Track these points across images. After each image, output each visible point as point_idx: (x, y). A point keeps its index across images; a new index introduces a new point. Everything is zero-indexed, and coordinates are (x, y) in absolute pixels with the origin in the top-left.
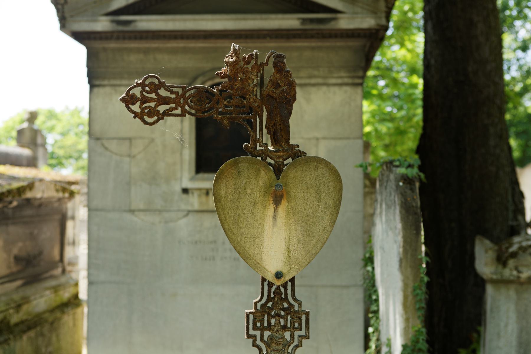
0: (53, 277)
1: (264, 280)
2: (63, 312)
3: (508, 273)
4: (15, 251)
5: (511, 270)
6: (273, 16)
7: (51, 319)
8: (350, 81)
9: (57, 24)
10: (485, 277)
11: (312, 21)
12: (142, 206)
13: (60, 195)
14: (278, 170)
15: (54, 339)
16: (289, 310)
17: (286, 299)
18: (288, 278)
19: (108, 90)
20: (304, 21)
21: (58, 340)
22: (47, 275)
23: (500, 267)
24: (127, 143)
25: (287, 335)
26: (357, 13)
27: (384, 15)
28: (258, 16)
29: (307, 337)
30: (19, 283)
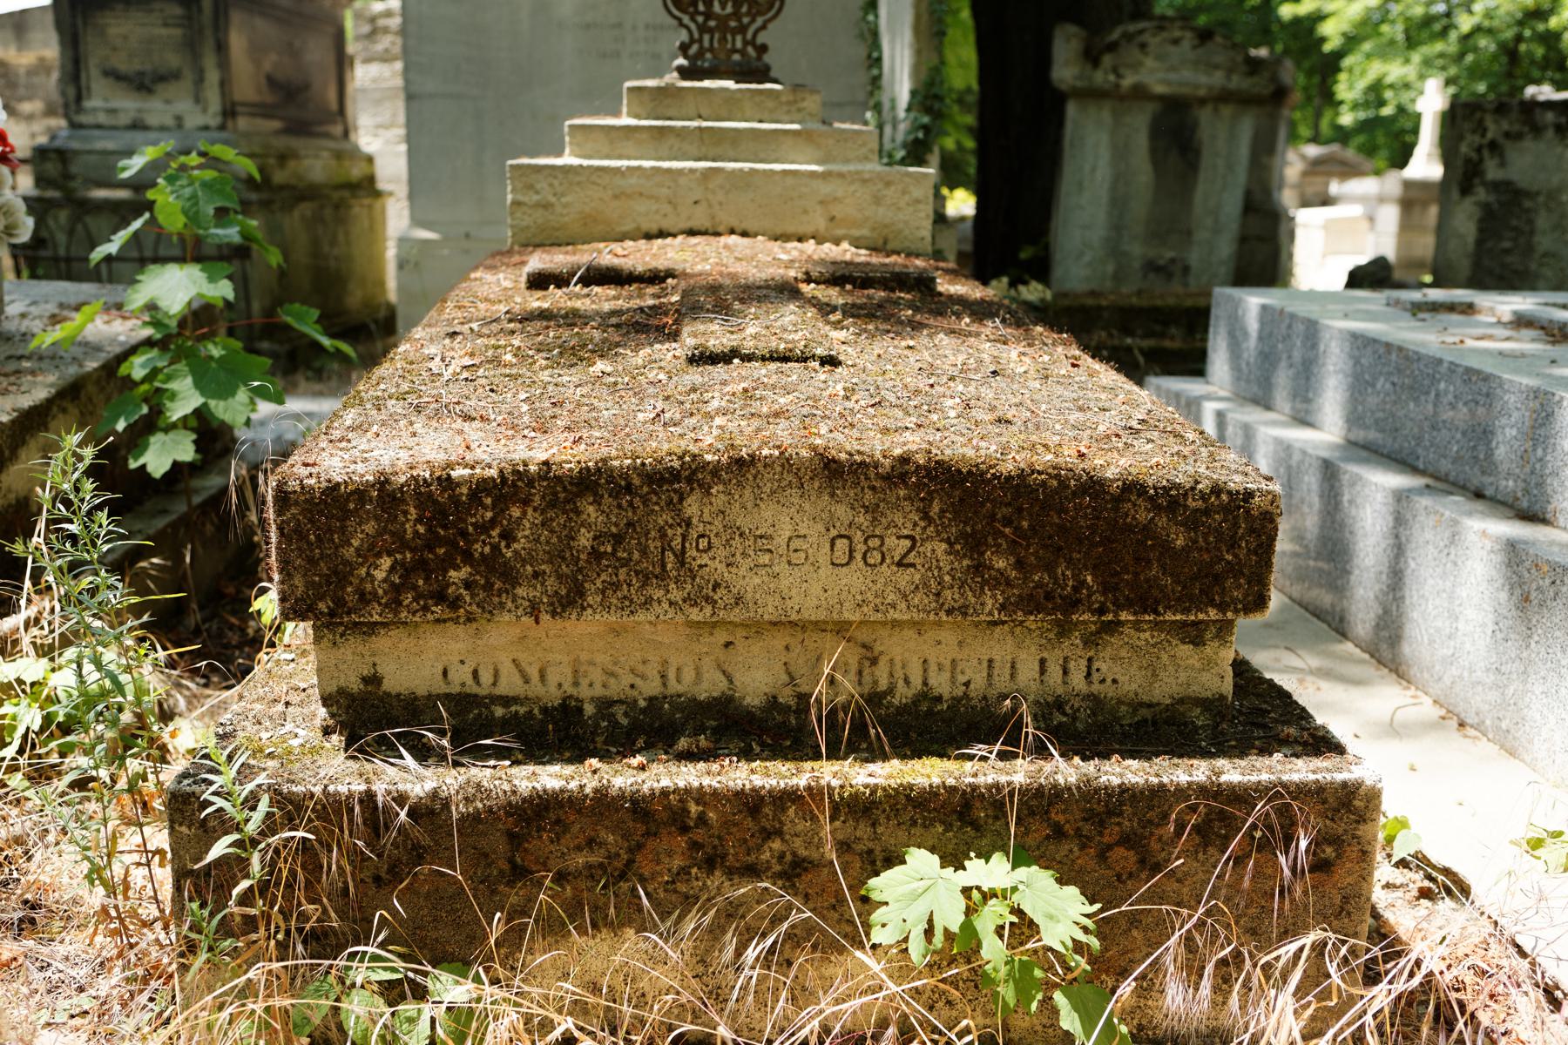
0: (327, 136)
2: (354, 196)
3: (1102, 77)
4: (267, 66)
5: (1106, 73)
10: (1063, 87)
15: (341, 237)
30: (276, 124)
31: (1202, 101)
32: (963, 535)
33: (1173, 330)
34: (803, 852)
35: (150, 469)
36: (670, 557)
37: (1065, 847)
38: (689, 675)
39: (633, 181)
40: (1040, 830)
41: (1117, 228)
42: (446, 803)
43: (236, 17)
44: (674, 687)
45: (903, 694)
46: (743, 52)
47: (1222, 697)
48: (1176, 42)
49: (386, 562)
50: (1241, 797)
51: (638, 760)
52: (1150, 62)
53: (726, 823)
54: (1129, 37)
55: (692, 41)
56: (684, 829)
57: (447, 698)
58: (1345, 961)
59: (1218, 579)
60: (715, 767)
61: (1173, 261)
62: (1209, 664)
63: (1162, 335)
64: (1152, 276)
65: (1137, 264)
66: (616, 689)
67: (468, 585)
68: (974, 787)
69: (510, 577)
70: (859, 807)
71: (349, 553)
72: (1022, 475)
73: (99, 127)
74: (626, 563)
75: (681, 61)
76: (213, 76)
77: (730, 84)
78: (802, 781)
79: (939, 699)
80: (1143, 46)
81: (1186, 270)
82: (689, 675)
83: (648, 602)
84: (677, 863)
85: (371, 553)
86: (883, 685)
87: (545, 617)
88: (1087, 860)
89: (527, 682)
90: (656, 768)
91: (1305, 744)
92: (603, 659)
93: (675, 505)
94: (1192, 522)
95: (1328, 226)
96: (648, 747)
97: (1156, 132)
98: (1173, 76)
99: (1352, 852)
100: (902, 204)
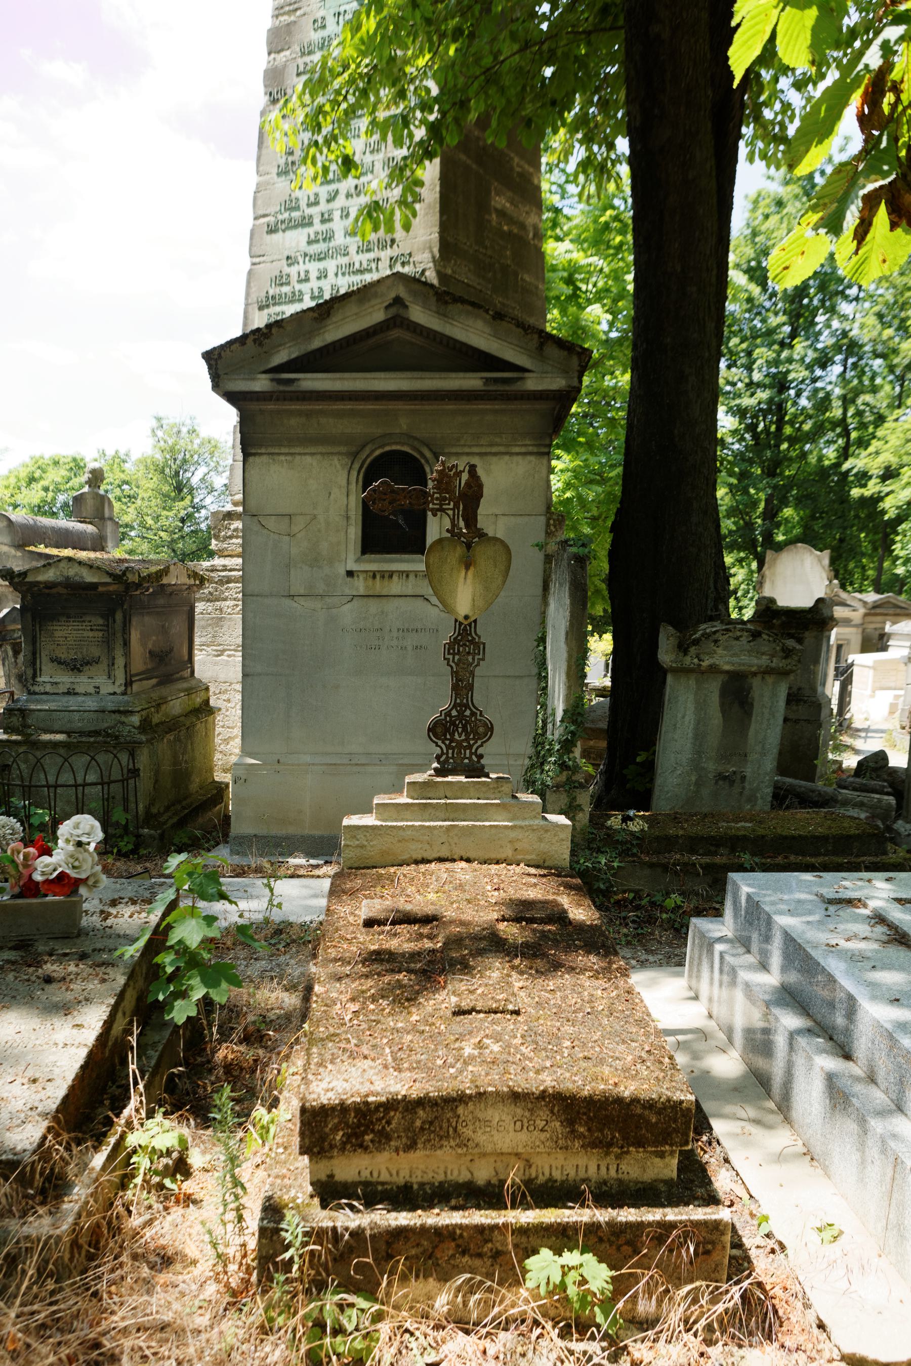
0: (183, 678)
1: (456, 620)
3: (689, 661)
4: (150, 646)
6: (453, 375)
7: (188, 724)
8: (535, 450)
9: (209, 383)
11: (496, 381)
12: (302, 592)
13: (192, 582)
14: (469, 546)
16: (472, 642)
17: (470, 634)
18: (473, 619)
19: (265, 459)
20: (487, 381)
21: (193, 750)
22: (178, 676)
23: (681, 654)
24: (287, 519)
25: (470, 658)
26: (546, 372)
27: (576, 374)
28: (437, 375)
29: (483, 659)
30: (154, 681)
31: (755, 674)
32: (566, 1119)
33: (722, 850)
34: (500, 1248)
35: (176, 1020)
36: (451, 1130)
37: (603, 1246)
38: (456, 1173)
39: (409, 833)
40: (593, 1239)
41: (698, 752)
42: (364, 1230)
43: (135, 621)
44: (449, 1177)
45: (541, 1179)
46: (470, 759)
47: (672, 1179)
48: (737, 639)
49: (341, 1133)
50: (672, 1225)
51: (436, 1211)
52: (720, 651)
53: (471, 1237)
54: (706, 636)
55: (443, 753)
56: (454, 1240)
57: (360, 1183)
58: (712, 1292)
59: (669, 1134)
60: (467, 1213)
61: (734, 773)
62: (667, 1166)
63: (715, 854)
64: (721, 782)
65: (711, 776)
66: (427, 1178)
67: (372, 1141)
68: (568, 1223)
69: (388, 1138)
70: (523, 1231)
71: (327, 1130)
72: (590, 1096)
73: (46, 693)
74: (433, 1132)
75: (435, 765)
76: (120, 662)
77: (462, 779)
78: (501, 1221)
79: (556, 1181)
80: (716, 641)
81: (743, 778)
82: (456, 1173)
83: (441, 1147)
84: (451, 1252)
85: (335, 1129)
86: (534, 1175)
87: (401, 1153)
88: (612, 1251)
89: (391, 1175)
90: (444, 1214)
91: (704, 1200)
92: (422, 1166)
93: (454, 1110)
94: (659, 1112)
95: (875, 667)
96: (440, 1202)
97: (723, 693)
98: (735, 659)
99: (719, 1247)
100: (554, 841)
